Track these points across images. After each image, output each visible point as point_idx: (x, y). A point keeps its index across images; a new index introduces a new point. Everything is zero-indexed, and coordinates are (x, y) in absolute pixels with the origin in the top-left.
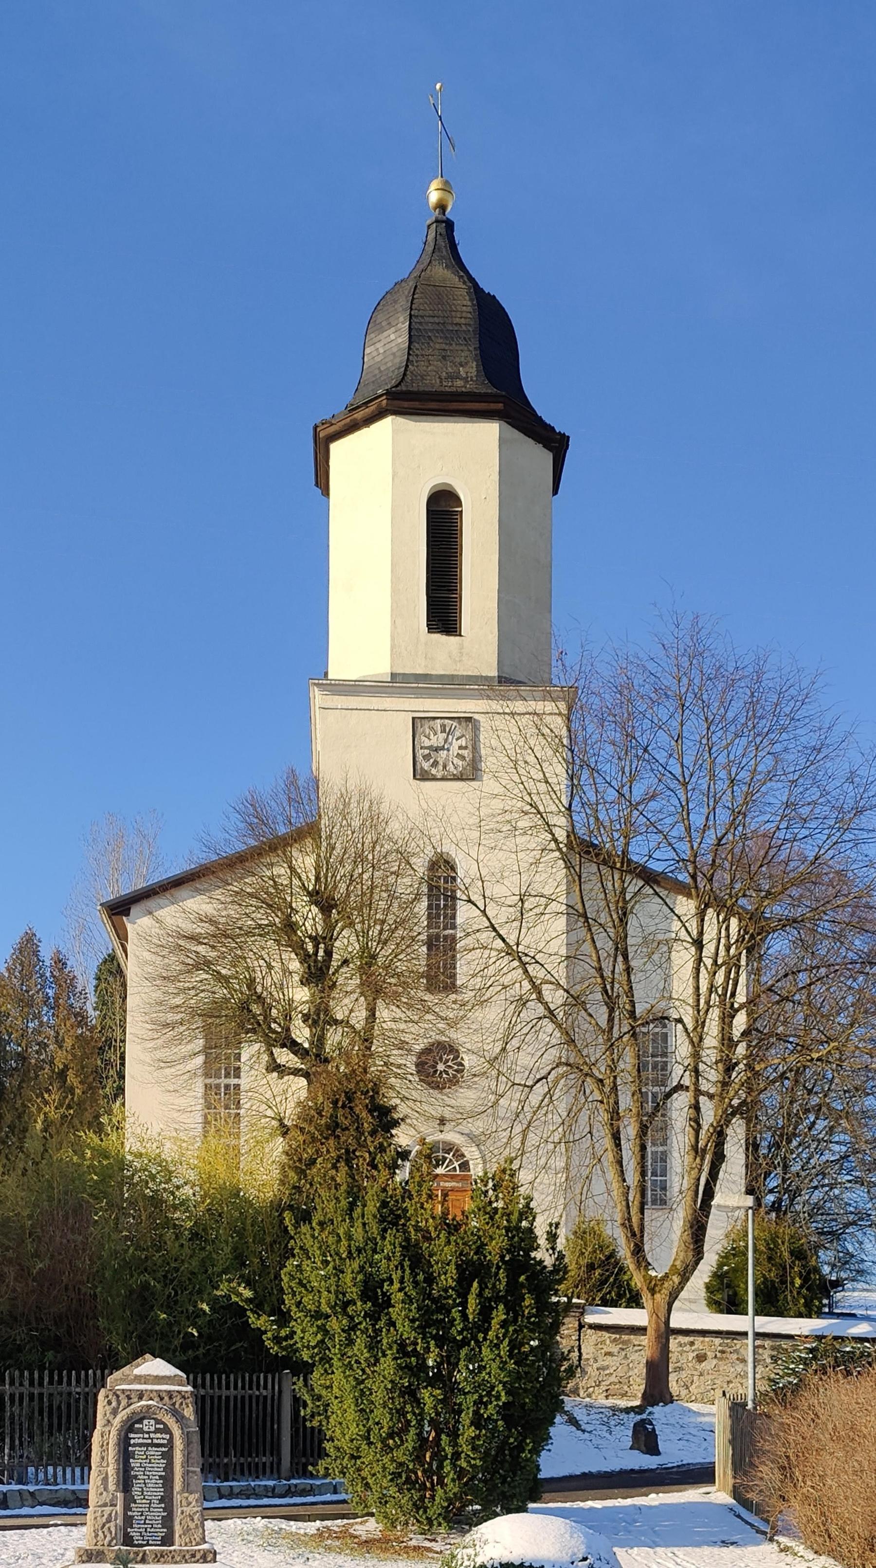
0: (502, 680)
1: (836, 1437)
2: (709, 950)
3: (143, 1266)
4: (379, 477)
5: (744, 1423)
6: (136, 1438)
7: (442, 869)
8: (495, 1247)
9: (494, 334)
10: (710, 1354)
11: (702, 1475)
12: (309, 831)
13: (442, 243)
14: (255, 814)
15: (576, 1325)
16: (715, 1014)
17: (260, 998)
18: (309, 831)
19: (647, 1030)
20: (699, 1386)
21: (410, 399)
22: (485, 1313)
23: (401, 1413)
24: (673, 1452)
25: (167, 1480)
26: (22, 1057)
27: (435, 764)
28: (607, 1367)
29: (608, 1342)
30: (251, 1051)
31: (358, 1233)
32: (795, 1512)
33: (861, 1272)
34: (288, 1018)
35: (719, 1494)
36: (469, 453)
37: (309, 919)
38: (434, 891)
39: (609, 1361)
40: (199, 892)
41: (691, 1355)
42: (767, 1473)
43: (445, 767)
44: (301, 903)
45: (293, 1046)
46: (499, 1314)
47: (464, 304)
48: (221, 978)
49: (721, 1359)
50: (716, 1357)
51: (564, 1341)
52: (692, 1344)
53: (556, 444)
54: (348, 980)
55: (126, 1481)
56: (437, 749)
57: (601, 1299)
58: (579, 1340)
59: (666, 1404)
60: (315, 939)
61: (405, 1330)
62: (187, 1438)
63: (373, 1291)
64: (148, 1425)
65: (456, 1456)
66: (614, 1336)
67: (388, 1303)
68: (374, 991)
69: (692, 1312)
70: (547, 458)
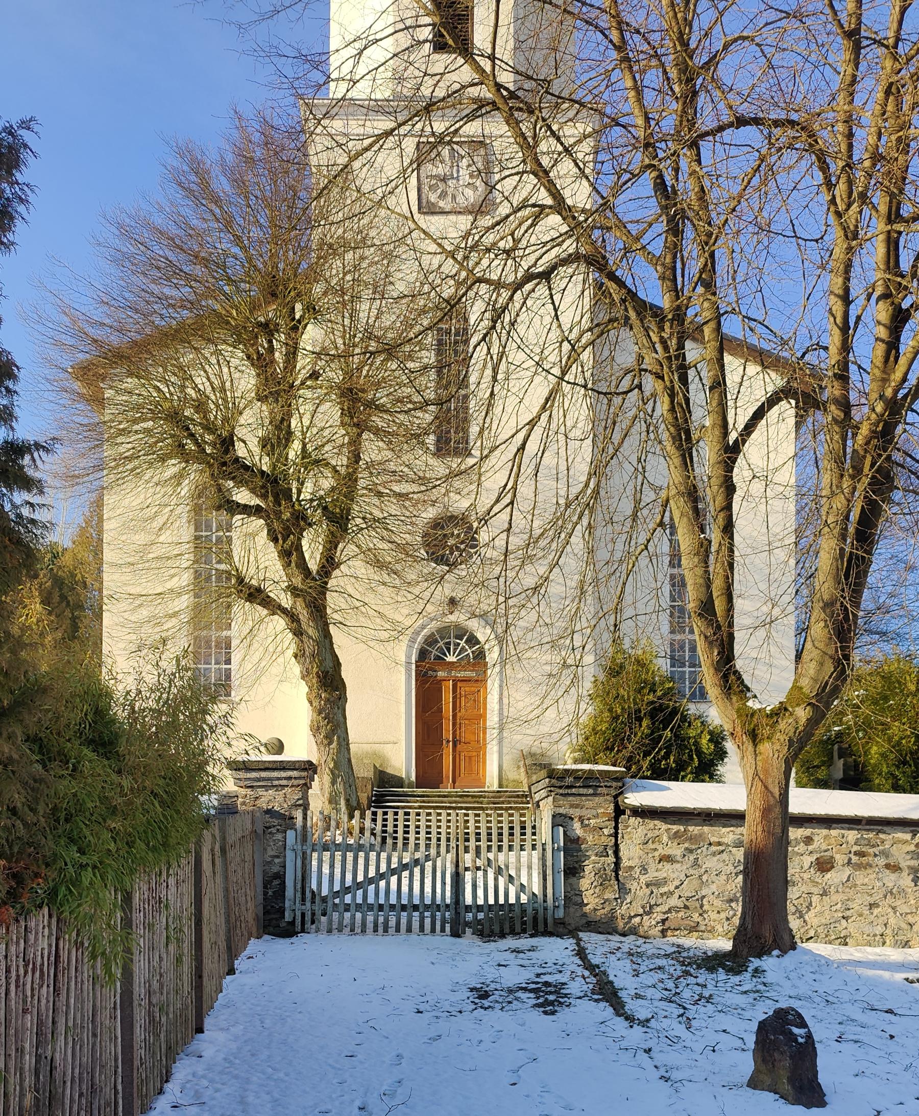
10: (840, 859)
15: (611, 808)
20: (821, 913)
27: (443, 195)
28: (665, 881)
29: (665, 838)
39: (667, 870)
41: (808, 860)
43: (454, 197)
49: (859, 867)
50: (849, 862)
51: (590, 838)
52: (808, 840)
56: (444, 180)
57: (652, 766)
58: (616, 835)
59: (784, 952)
66: (675, 828)
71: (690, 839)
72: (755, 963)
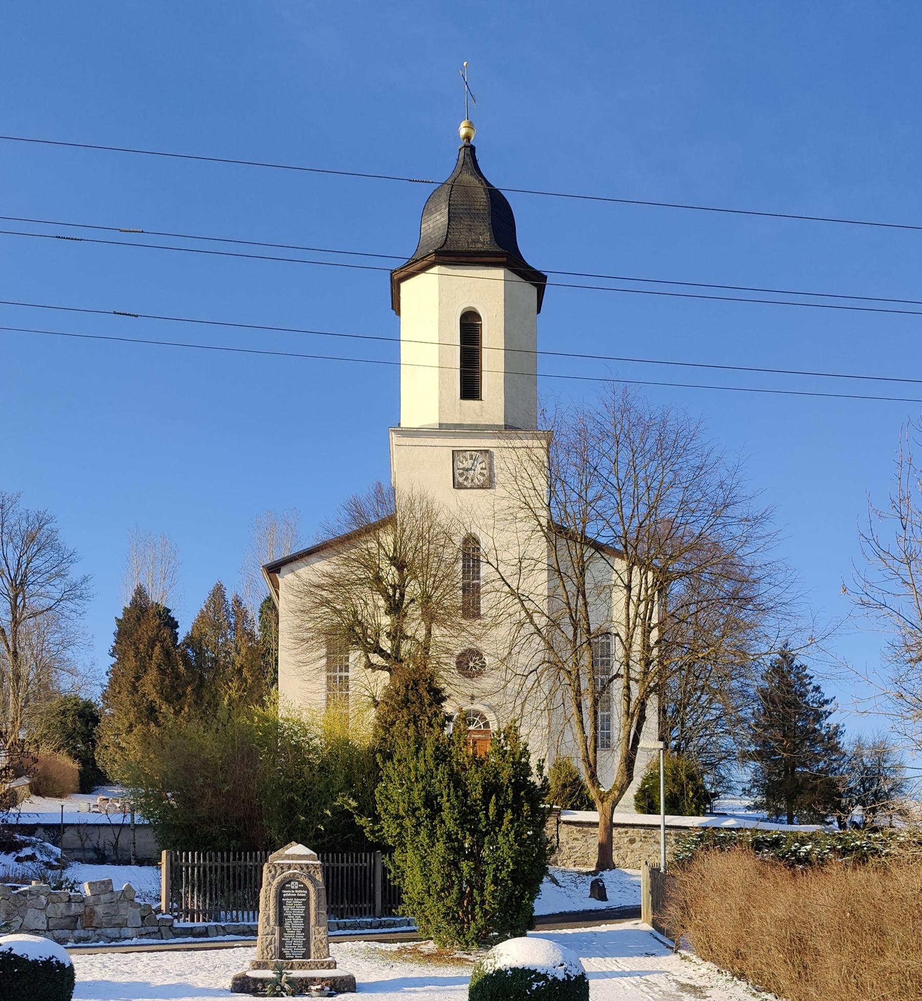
0: (507, 427)
1: (715, 889)
2: (635, 591)
3: (290, 788)
4: (429, 304)
5: (659, 882)
6: (286, 893)
8: (506, 774)
9: (500, 215)
10: (638, 839)
11: (633, 913)
12: (389, 521)
13: (468, 160)
14: (357, 511)
16: (639, 630)
17: (360, 623)
18: (389, 521)
21: (450, 255)
22: (500, 815)
23: (449, 876)
24: (615, 899)
25: (306, 919)
26: (215, 661)
27: (467, 479)
30: (355, 656)
32: (690, 935)
33: (729, 788)
34: (377, 635)
35: (644, 925)
36: (486, 289)
37: (390, 574)
38: (466, 557)
39: (576, 843)
40: (323, 558)
41: (626, 840)
42: (673, 911)
43: (472, 480)
45: (381, 652)
46: (508, 815)
47: (482, 197)
48: (338, 612)
49: (644, 842)
53: (537, 279)
54: (414, 611)
55: (281, 919)
56: (467, 470)
61: (451, 825)
62: (318, 892)
63: (430, 801)
65: (483, 902)
68: (430, 617)
69: (627, 813)
70: (534, 291)
71: (584, 832)
72: (601, 873)
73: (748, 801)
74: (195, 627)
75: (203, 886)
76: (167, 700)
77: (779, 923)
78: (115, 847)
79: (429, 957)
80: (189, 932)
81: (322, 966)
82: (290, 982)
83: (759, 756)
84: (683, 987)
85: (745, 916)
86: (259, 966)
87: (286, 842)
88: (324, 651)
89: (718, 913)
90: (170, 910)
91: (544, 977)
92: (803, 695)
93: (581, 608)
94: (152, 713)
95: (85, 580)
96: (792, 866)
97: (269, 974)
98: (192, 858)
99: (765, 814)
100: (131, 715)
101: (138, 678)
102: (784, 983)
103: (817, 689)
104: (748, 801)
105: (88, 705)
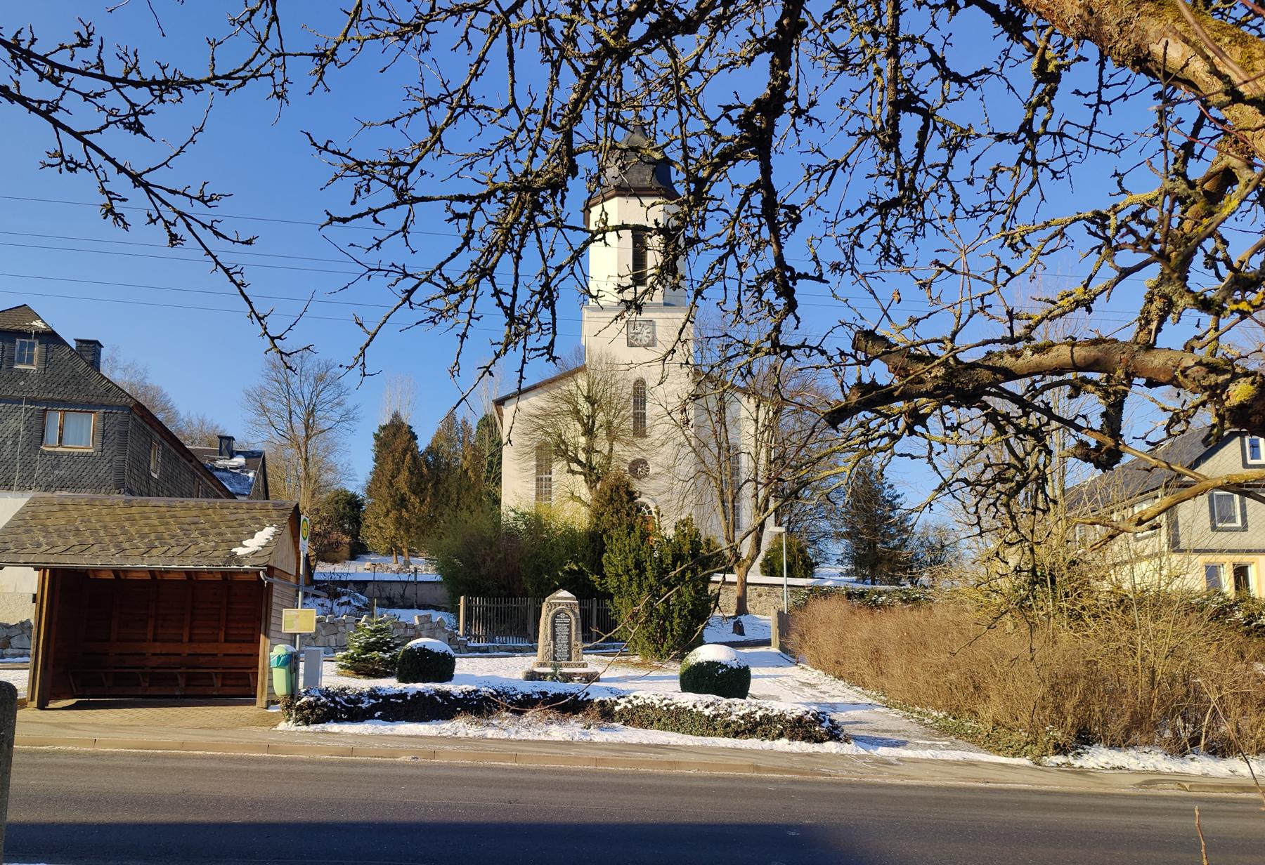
1: (822, 622)
2: (761, 421)
3: (536, 556)
5: (784, 622)
6: (558, 620)
7: (640, 386)
8: (686, 548)
11: (767, 643)
12: (582, 369)
16: (764, 450)
17: (564, 442)
19: (729, 453)
24: (750, 635)
25: (569, 636)
26: (448, 464)
30: (559, 467)
31: (633, 544)
32: (807, 652)
33: (826, 559)
34: (576, 449)
35: (774, 649)
37: (585, 408)
42: (795, 637)
44: (581, 400)
45: (579, 463)
54: (602, 433)
55: (554, 637)
60: (588, 417)
61: (652, 581)
64: (562, 615)
65: (672, 630)
67: (645, 570)
69: (755, 576)
73: (841, 569)
74: (434, 440)
75: (486, 622)
76: (414, 493)
77: (865, 642)
78: (402, 596)
79: (637, 665)
80: (477, 649)
81: (579, 666)
82: (561, 674)
83: (848, 535)
84: (803, 684)
85: (841, 640)
86: (542, 665)
87: (556, 589)
88: (534, 463)
89: (825, 639)
90: (465, 635)
91: (726, 666)
92: (880, 491)
93: (723, 434)
94: (402, 502)
95: (356, 407)
96: (872, 608)
97: (549, 670)
98: (478, 601)
99: (855, 578)
100: (388, 504)
101: (393, 477)
102: (867, 678)
103: (891, 486)
104: (841, 569)
105: (354, 496)
